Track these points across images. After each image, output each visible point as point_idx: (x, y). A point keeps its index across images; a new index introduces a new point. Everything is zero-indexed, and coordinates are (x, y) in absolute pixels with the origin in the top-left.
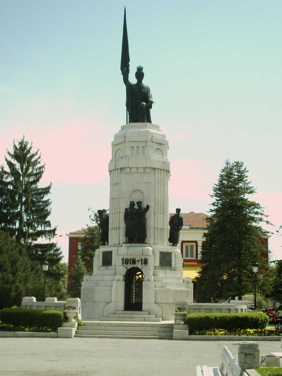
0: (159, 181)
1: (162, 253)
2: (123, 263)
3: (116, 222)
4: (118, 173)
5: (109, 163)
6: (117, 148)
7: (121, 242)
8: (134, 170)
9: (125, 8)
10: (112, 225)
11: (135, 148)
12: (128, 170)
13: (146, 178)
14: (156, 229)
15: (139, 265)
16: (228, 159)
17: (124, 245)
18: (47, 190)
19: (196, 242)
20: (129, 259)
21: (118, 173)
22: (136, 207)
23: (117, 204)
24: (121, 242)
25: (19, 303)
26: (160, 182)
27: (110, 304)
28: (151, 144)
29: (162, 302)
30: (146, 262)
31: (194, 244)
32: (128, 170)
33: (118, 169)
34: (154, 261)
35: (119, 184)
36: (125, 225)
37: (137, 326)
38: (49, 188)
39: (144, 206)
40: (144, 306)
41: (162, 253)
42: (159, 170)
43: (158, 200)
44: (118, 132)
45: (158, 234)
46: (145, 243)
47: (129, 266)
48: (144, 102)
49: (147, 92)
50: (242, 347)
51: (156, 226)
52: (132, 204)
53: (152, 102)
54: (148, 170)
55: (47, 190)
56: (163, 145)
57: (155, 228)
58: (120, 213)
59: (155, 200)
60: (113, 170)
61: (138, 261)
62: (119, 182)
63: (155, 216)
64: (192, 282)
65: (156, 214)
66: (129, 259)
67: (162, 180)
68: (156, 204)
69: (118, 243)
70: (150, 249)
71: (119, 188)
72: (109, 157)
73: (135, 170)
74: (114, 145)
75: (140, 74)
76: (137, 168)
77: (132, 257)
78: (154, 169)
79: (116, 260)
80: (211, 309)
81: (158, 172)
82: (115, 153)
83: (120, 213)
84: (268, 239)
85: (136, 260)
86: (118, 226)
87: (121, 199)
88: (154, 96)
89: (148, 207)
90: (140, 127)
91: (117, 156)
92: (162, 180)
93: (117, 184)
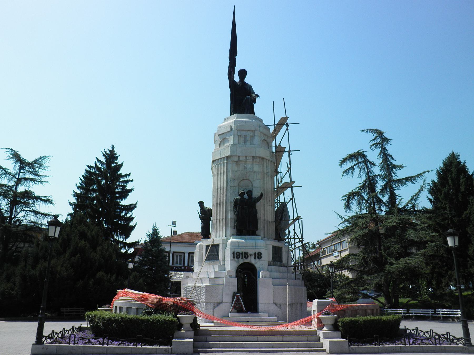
2: (234, 257)
3: (221, 213)
9: (234, 9)
15: (252, 260)
18: (132, 207)
19: (184, 253)
22: (246, 196)
27: (221, 305)
30: (259, 256)
31: (183, 255)
33: (224, 158)
34: (267, 255)
38: (136, 204)
46: (257, 235)
47: (241, 261)
49: (250, 89)
50: (322, 347)
51: (266, 218)
55: (132, 207)
61: (251, 255)
63: (264, 207)
65: (266, 206)
66: (240, 252)
75: (243, 73)
77: (244, 250)
79: (226, 255)
85: (249, 254)
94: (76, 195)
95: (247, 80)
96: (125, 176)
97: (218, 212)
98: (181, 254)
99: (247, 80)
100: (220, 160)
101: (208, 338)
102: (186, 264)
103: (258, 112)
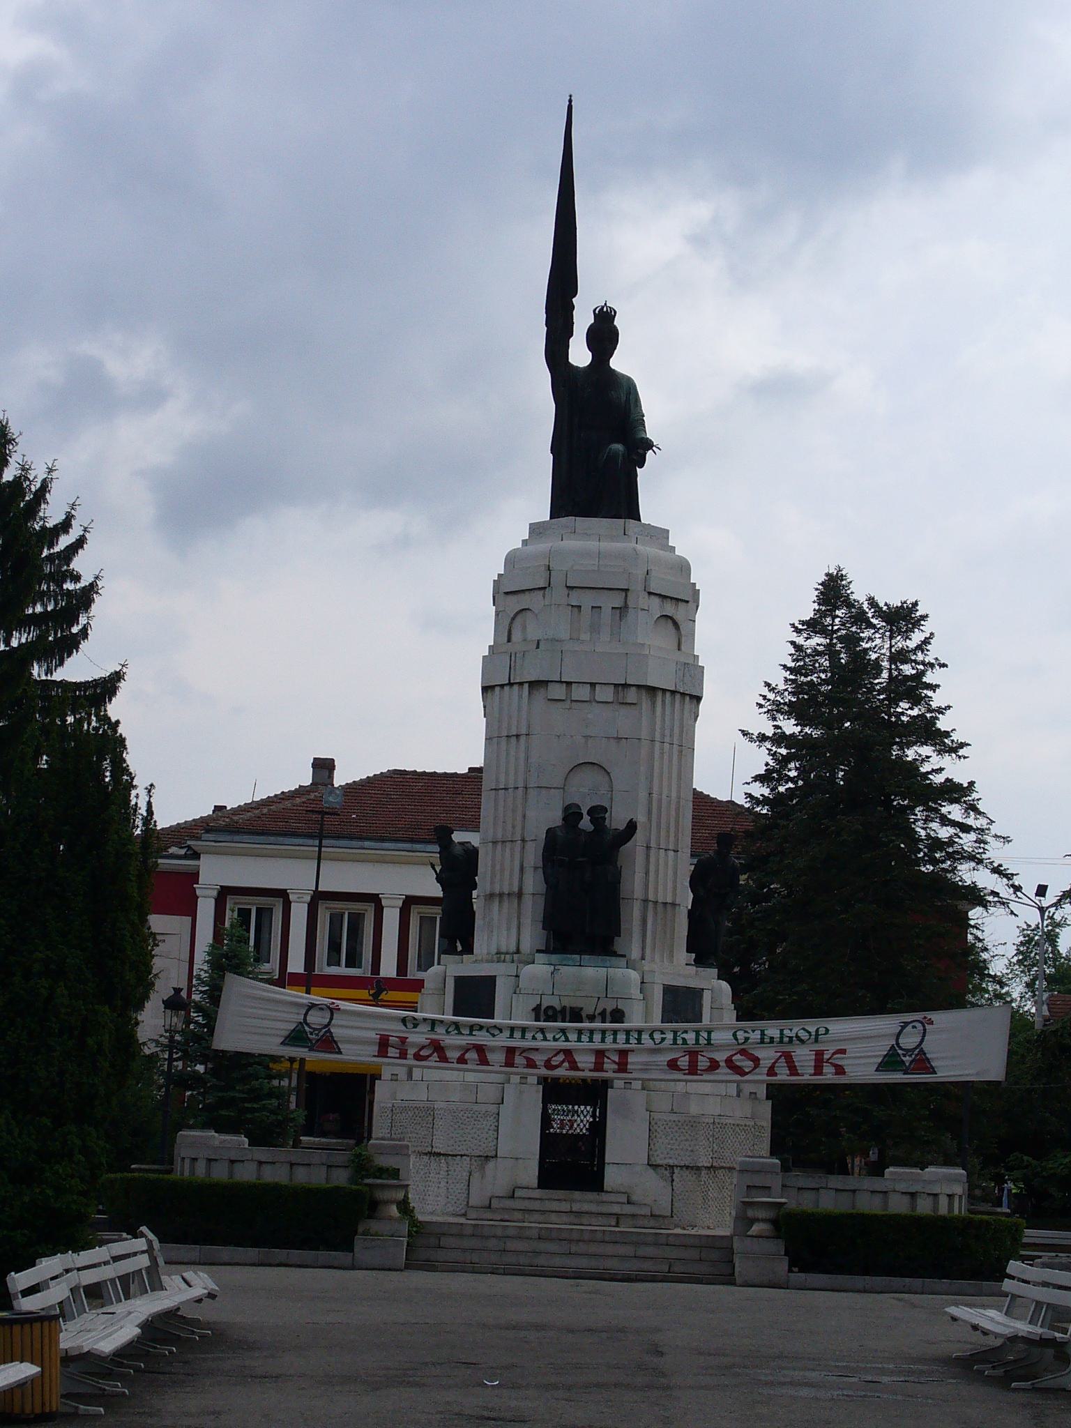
0: (667, 732)
1: (669, 991)
3: (507, 873)
4: (520, 697)
5: (484, 657)
6: (514, 604)
7: (526, 946)
8: (582, 693)
9: (570, 101)
10: (492, 883)
11: (586, 609)
12: (558, 692)
13: (623, 721)
14: (651, 905)
16: (962, 745)
17: (540, 957)
18: (108, 687)
19: (374, 899)
20: (558, 1008)
21: (520, 697)
22: (586, 823)
23: (514, 811)
24: (526, 946)
25: (166, 1156)
26: (667, 739)
28: (644, 601)
29: (671, 1162)
32: (558, 692)
33: (521, 684)
34: (644, 1014)
35: (523, 739)
36: (542, 888)
37: (607, 1239)
38: (117, 677)
39: (617, 820)
40: (612, 1177)
41: (669, 991)
42: (668, 694)
43: (660, 801)
44: (520, 546)
45: (655, 920)
46: (615, 954)
48: (618, 442)
49: (628, 400)
51: (651, 897)
52: (571, 815)
53: (649, 445)
54: (632, 696)
55: (108, 687)
56: (681, 605)
57: (646, 901)
58: (523, 840)
59: (650, 802)
60: (502, 686)
62: (524, 731)
63: (648, 856)
64: (767, 1098)
65: (653, 852)
66: (558, 1008)
67: (676, 731)
68: (654, 816)
69: (513, 948)
70: (634, 975)
71: (522, 756)
72: (483, 635)
73: (605, 694)
74: (503, 592)
75: (604, 334)
76: (593, 685)
78: (652, 690)
80: (854, 1191)
81: (663, 701)
82: (507, 623)
83: (523, 840)
84: (541, 510)
86: (516, 889)
87: (532, 793)
88: (657, 415)
89: (632, 827)
90: (592, 538)
91: (517, 636)
92: (676, 731)
93: (518, 736)
94: (209, 954)
95: (617, 363)
96: (65, 526)
97: (498, 867)
98: (356, 907)
99: (617, 363)
100: (506, 688)
101: (445, 1241)
102: (389, 968)
103: (651, 508)
